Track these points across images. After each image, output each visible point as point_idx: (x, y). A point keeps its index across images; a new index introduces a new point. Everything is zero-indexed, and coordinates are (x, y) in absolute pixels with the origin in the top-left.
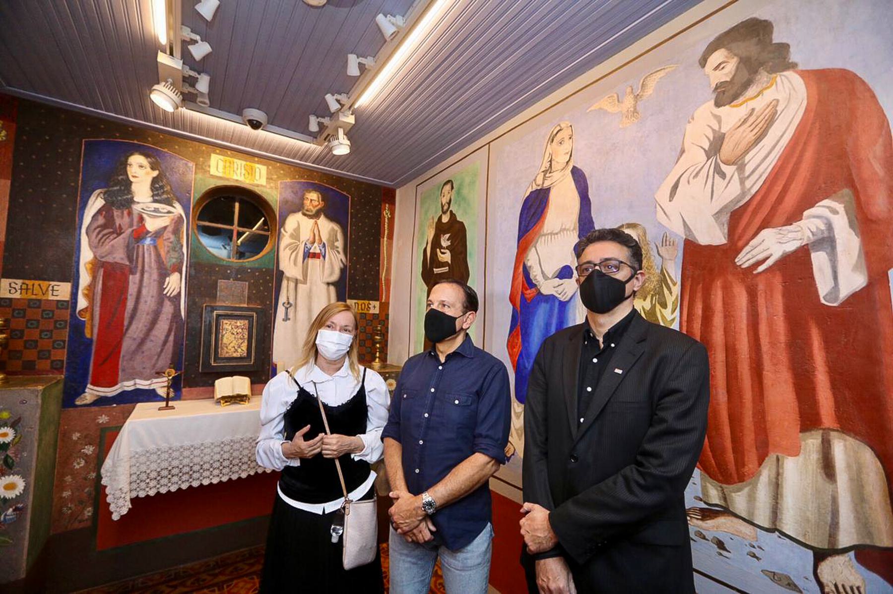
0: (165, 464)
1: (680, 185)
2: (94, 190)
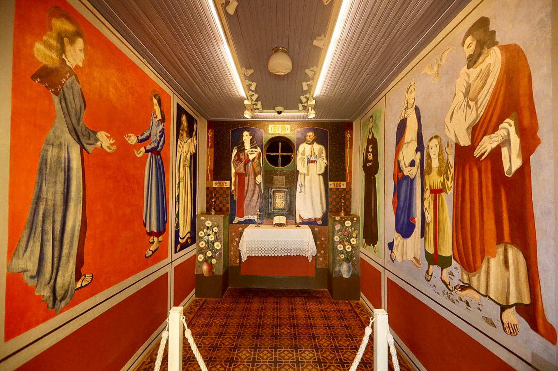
0: (257, 246)
1: (454, 113)
2: (234, 147)
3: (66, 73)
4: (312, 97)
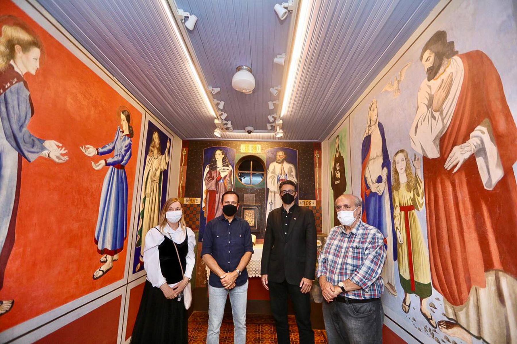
1: (418, 126)
3: (13, 79)
4: (279, 117)
